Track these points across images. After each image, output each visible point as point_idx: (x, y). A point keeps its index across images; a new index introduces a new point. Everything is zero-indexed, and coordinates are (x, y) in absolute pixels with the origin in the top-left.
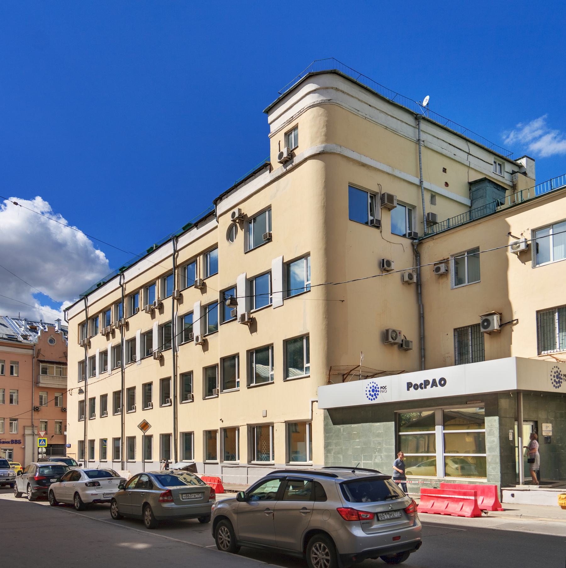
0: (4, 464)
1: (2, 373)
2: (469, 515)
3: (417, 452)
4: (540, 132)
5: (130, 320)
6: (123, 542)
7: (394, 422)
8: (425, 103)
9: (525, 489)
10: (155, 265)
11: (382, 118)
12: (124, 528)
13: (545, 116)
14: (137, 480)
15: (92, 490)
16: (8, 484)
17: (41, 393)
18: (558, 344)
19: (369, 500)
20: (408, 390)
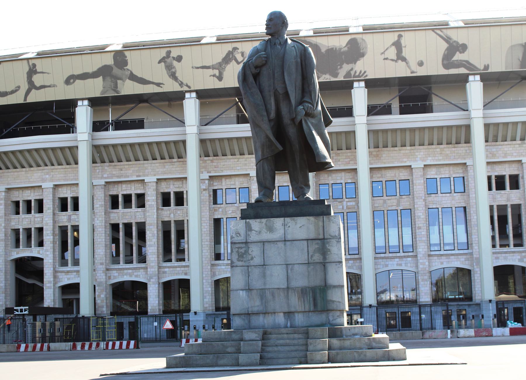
0: (318, 208)
1: (466, 364)
2: (296, 315)
3: (343, 286)
4: (259, 339)
5: (482, 67)
6: (316, 130)
7: (165, 359)
8: (343, 57)
9: (502, 118)
10: (409, 365)
11: (225, 226)
12: (493, 229)
13: (105, 312)
14: (462, 71)
15: (509, 230)
16: (229, 319)
17: (240, 238)
18: (65, 316)
19: (272, 124)
20: (160, 62)
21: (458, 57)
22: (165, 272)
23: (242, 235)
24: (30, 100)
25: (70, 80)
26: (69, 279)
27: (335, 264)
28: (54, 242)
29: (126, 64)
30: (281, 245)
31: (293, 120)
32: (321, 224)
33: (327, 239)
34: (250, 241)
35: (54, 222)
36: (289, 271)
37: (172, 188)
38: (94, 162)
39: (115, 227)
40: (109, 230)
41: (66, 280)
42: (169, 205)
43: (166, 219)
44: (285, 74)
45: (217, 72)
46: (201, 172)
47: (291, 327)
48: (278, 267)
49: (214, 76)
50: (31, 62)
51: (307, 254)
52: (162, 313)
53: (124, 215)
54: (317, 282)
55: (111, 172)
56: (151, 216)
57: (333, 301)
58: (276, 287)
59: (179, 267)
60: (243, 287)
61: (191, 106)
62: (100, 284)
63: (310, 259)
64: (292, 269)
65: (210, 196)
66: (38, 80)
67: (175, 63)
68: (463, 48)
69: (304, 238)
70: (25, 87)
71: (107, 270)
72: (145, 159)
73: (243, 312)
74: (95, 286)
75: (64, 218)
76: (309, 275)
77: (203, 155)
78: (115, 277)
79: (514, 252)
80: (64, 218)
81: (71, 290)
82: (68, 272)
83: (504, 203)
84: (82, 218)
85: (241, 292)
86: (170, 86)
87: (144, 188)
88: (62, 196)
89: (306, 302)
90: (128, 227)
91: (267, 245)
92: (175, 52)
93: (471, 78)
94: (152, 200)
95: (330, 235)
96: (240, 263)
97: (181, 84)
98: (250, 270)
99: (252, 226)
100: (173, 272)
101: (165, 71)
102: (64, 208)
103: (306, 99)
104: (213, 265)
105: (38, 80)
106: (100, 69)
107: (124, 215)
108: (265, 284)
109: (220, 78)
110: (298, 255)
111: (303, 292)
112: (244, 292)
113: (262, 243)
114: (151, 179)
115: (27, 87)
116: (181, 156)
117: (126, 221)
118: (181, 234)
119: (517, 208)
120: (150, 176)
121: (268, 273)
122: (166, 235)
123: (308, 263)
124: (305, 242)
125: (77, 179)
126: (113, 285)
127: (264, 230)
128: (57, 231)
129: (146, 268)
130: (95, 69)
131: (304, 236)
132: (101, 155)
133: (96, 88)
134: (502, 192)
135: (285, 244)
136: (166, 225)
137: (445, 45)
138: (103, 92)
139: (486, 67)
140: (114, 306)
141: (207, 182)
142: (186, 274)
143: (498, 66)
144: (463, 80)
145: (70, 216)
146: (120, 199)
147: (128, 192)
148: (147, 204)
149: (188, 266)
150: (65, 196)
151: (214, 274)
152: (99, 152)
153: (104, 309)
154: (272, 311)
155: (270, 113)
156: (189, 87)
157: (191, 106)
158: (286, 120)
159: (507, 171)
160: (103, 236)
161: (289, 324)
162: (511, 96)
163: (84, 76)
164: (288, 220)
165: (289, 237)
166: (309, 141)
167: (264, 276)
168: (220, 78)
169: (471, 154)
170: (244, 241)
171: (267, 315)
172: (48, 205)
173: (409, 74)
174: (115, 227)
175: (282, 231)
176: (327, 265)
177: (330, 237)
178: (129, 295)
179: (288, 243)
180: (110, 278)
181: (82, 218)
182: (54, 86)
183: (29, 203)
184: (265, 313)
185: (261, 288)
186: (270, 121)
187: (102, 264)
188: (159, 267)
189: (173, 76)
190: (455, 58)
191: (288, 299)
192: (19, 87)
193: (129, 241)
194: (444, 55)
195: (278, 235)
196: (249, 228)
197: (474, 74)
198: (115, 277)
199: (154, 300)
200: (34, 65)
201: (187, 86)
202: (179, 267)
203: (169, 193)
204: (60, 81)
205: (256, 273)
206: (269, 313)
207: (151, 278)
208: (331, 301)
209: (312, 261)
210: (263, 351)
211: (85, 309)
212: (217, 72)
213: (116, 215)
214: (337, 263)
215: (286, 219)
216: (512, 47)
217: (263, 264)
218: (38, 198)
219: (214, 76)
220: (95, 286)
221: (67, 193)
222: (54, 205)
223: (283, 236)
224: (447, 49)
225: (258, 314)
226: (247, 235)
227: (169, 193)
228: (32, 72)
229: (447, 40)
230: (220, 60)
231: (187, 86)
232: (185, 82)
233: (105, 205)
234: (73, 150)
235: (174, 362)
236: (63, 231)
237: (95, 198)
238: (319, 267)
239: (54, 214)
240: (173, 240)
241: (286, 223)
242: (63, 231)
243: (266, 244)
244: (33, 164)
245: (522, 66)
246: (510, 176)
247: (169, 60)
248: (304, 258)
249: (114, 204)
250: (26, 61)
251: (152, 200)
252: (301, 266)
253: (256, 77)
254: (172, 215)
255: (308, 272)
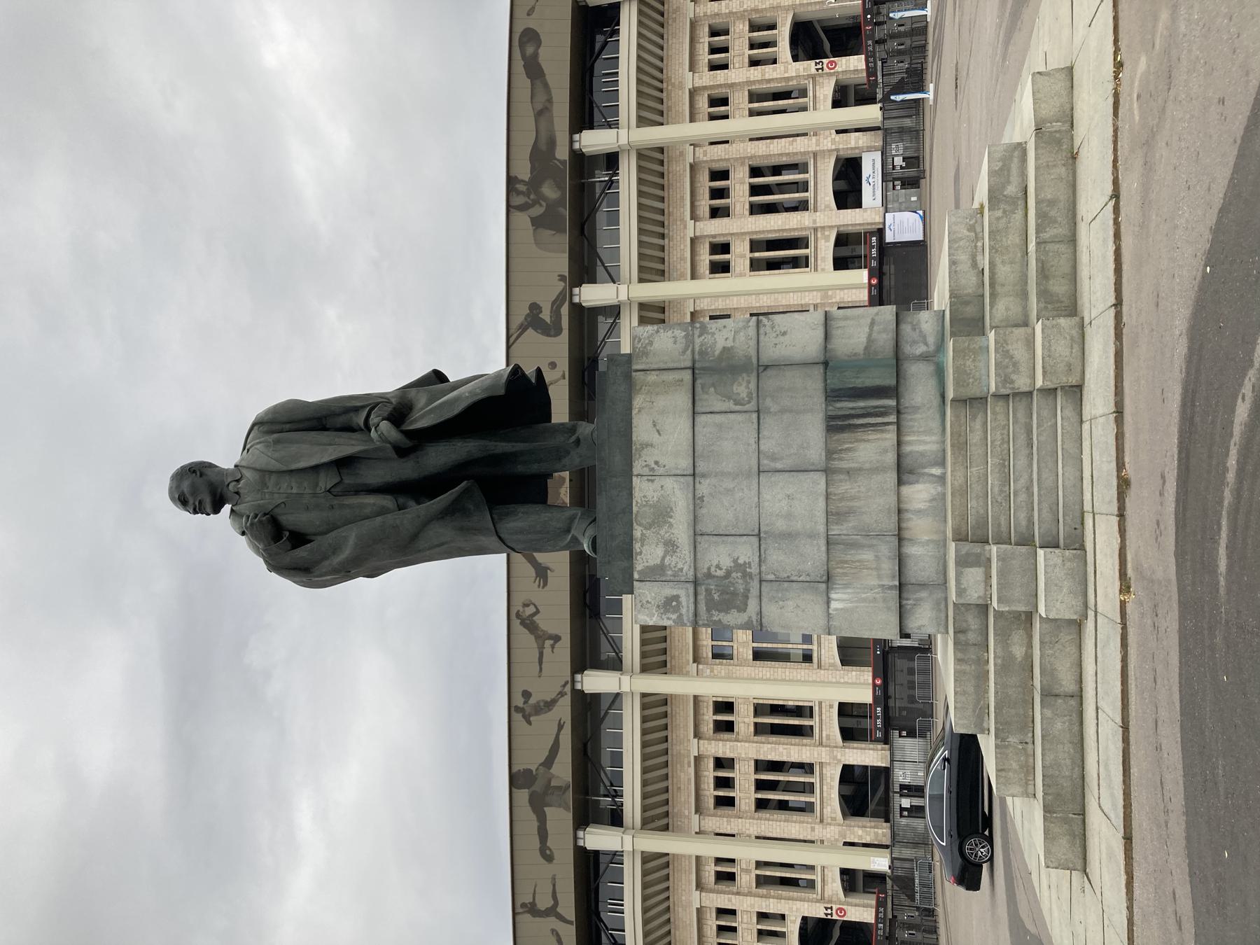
14: (565, 310)
20: (529, 723)
21: (546, 315)
22: (828, 736)
23: (675, 593)
24: (571, 915)
25: (547, 855)
26: (834, 881)
27: (762, 337)
28: (780, 898)
29: (530, 771)
30: (704, 488)
31: (402, 452)
32: (652, 377)
33: (694, 361)
34: (691, 573)
35: (749, 894)
36: (779, 466)
37: (709, 717)
38: (666, 828)
39: (761, 805)
40: (765, 814)
41: (835, 886)
42: (732, 723)
43: (752, 729)
44: (294, 467)
45: (548, 643)
46: (687, 674)
47: (942, 463)
48: (766, 496)
49: (553, 647)
50: (519, 910)
51: (732, 416)
52: (887, 747)
53: (745, 792)
54: (812, 386)
55: (684, 800)
56: (747, 750)
57: (870, 340)
58: (821, 503)
59: (821, 715)
60: (821, 599)
61: (596, 682)
62: (842, 835)
63: (747, 407)
64: (773, 458)
65: (721, 664)
66: (544, 903)
67: (532, 701)
68: (535, 308)
69: (688, 424)
70: (552, 922)
71: (822, 821)
72: (666, 752)
73: (894, 605)
74: (846, 844)
75: (746, 879)
76: (791, 411)
77: (664, 670)
78: (833, 811)
79: (816, 248)
80: (746, 879)
81: (852, 880)
82: (823, 880)
83: (748, 262)
84: (746, 854)
85: (834, 605)
86: (564, 710)
87: (708, 757)
88: (712, 878)
89: (865, 437)
90: (761, 785)
91: (704, 527)
92: (519, 701)
93: (576, 300)
94: (723, 747)
95: (684, 352)
96: (752, 605)
97: (562, 694)
98: (771, 577)
99: (651, 563)
100: (829, 724)
101: (542, 717)
102: (731, 877)
103: (360, 420)
104: (819, 667)
105: (544, 903)
106: (535, 811)
107: (745, 792)
108: (812, 536)
109: (557, 638)
110: (732, 438)
111: (837, 425)
112: (833, 596)
113: (699, 538)
114: (693, 747)
115: (553, 919)
116: (664, 700)
117: (753, 788)
118: (777, 709)
119: (755, 245)
120: (694, 747)
121: (781, 525)
122: (777, 730)
123: (758, 411)
124: (701, 419)
125: (690, 856)
126: (844, 815)
127: (662, 532)
128: (763, 891)
129: (821, 764)
130: (534, 817)
131: (684, 424)
132: (658, 817)
133: (560, 817)
134: (732, 264)
135: (703, 476)
136: (759, 730)
137: (530, 331)
138: (567, 809)
139: (562, 278)
140: (875, 815)
141: (701, 667)
142: (831, 706)
143: (561, 263)
144: (577, 309)
145: (742, 870)
146: (721, 793)
147: (712, 781)
148: (729, 755)
149: (820, 703)
150: (713, 873)
151: (833, 665)
152: (653, 819)
153: (880, 831)
154: (895, 518)
155: (383, 507)
156: (566, 683)
157: (596, 682)
158: (406, 470)
159: (705, 258)
160: (777, 824)
161: (936, 471)
162: (603, 246)
163: (543, 834)
164: (637, 467)
165: (685, 463)
166: (456, 412)
167: (789, 536)
168: (557, 638)
169: (678, 302)
170: (691, 588)
171: (906, 534)
172: (725, 902)
173: (566, 381)
174: (761, 805)
175: (669, 483)
176: (765, 360)
177: (689, 352)
178: (863, 793)
179: (702, 466)
180: (834, 819)
181: (746, 854)
182: (554, 879)
183: (721, 929)
184: (900, 539)
185: (824, 548)
186: (401, 508)
187: (813, 829)
188: (821, 744)
189: (550, 705)
190: (548, 320)
191: (860, 469)
192: (553, 931)
193: (781, 786)
194: (542, 334)
195: (678, 493)
196: (656, 574)
197: (571, 295)
198: (833, 811)
199: (868, 756)
200: (523, 905)
201: (564, 686)
202: (821, 715)
203: (716, 722)
204: (547, 870)
205: (778, 558)
206: (900, 529)
207: (835, 758)
208: (866, 348)
209: (754, 402)
210: (1026, 541)
211: (879, 863)
212: (548, 643)
213: (743, 802)
214: (761, 331)
215: (635, 471)
216: (537, 243)
217: (755, 540)
218: (714, 915)
219: (553, 647)
220: (846, 844)
221: (710, 870)
222: (724, 893)
223: (682, 479)
224: (535, 330)
225: (901, 560)
226: (676, 580)
227: (716, 722)
228: (532, 909)
229: (523, 328)
230: (532, 637)
231: (564, 686)
232: (560, 689)
233: (729, 816)
234: (647, 858)
235: (1064, 846)
236: (762, 881)
237: (718, 831)
238: (771, 381)
239: (738, 893)
240: (785, 720)
241: (646, 471)
242: (762, 881)
243: (700, 528)
244: (665, 917)
245: (562, 231)
246: (711, 254)
247: (528, 710)
248: (743, 426)
249: (728, 802)
250: (518, 918)
251: (723, 747)
252: (764, 433)
253: (299, 539)
254: (746, 720)
255: (783, 411)
